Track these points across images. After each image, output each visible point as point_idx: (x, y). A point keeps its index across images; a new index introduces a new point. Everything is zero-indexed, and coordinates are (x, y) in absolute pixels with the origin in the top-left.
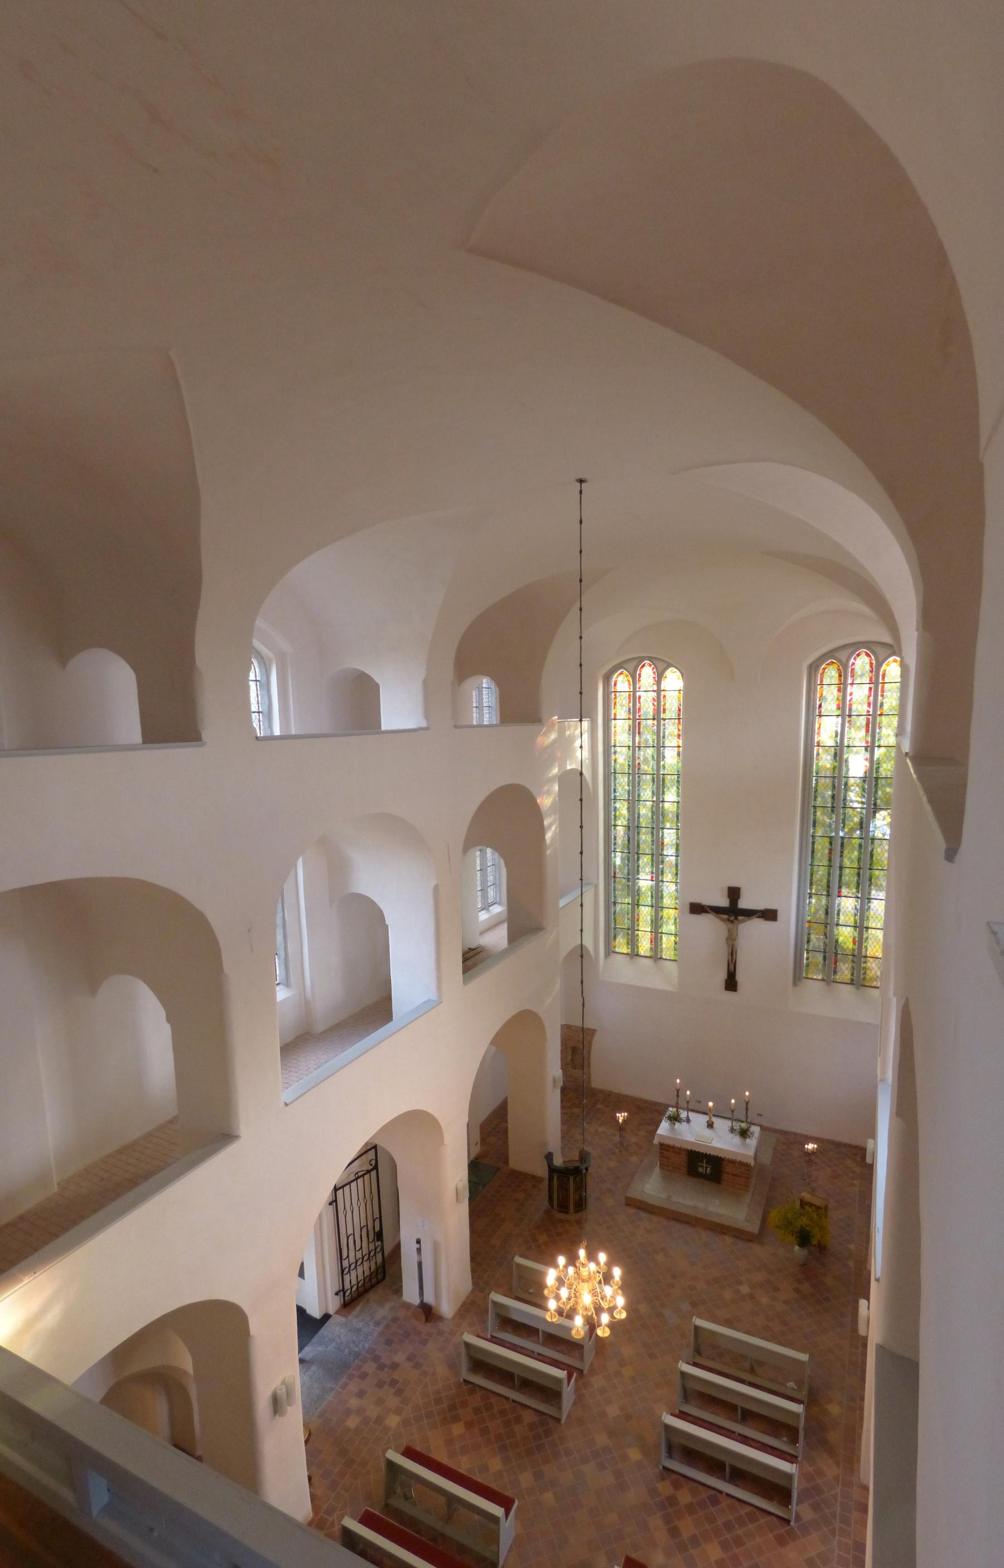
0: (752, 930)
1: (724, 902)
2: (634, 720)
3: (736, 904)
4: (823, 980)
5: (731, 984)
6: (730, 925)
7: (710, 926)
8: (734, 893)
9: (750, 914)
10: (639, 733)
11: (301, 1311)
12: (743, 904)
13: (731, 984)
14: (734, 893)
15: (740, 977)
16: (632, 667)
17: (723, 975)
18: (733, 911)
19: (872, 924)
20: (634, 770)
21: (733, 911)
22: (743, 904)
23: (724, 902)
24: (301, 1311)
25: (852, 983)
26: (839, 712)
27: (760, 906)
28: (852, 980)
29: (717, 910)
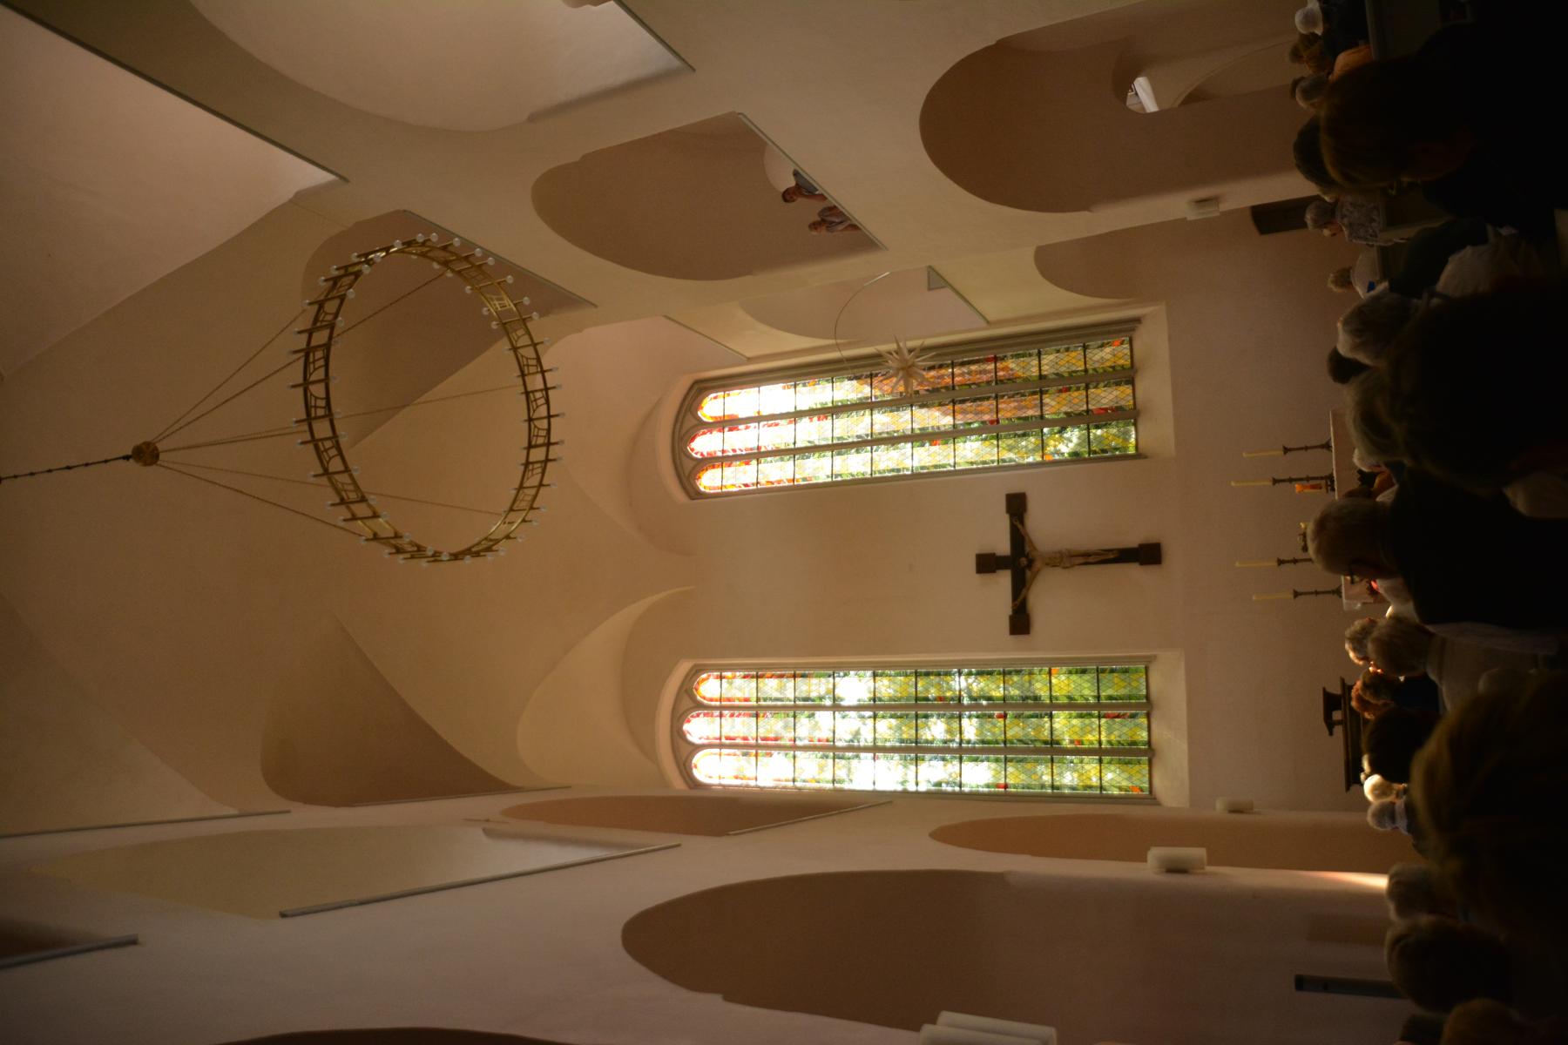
0: (1044, 529)
1: (1004, 580)
2: (757, 747)
3: (1005, 558)
4: (1135, 424)
5: (1149, 554)
6: (1038, 564)
7: (1047, 595)
8: (987, 564)
9: (1018, 537)
10: (776, 739)
11: (814, 226)
12: (1003, 547)
13: (1149, 554)
14: (987, 564)
15: (1132, 540)
16: (684, 751)
17: (1133, 570)
18: (1017, 563)
19: (1034, 372)
20: (751, 747)
21: (1017, 563)
22: (1003, 547)
23: (1004, 580)
24: (814, 226)
25: (1131, 381)
26: (754, 462)
27: (1004, 522)
28: (1127, 383)
29: (1020, 587)
